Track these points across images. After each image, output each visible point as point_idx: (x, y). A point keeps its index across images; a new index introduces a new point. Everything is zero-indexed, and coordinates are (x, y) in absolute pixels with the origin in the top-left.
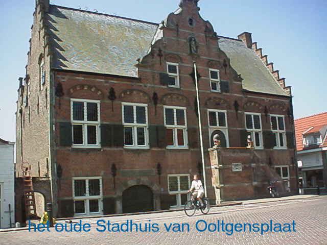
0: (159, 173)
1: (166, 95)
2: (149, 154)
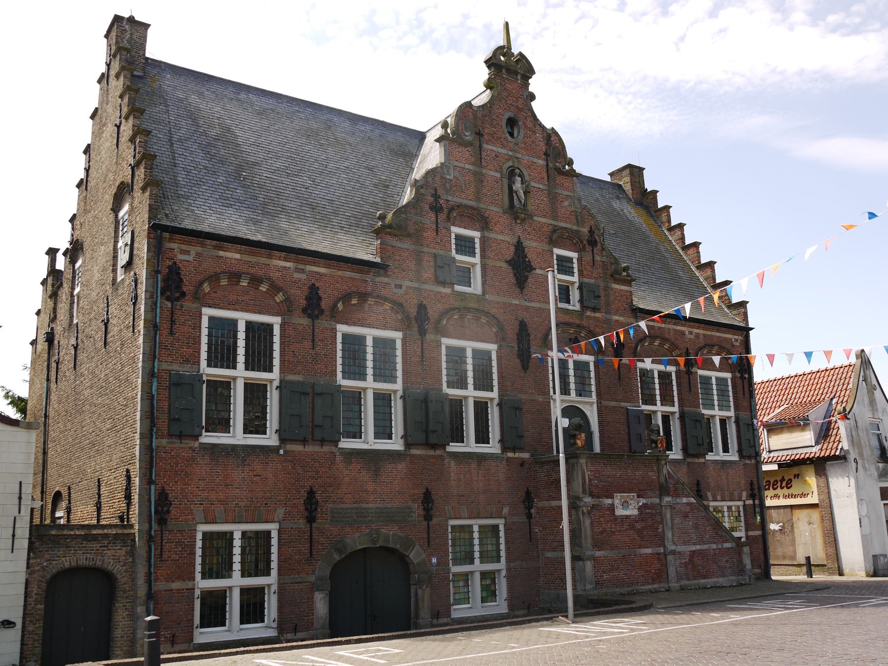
0: (428, 517)
2: (401, 466)
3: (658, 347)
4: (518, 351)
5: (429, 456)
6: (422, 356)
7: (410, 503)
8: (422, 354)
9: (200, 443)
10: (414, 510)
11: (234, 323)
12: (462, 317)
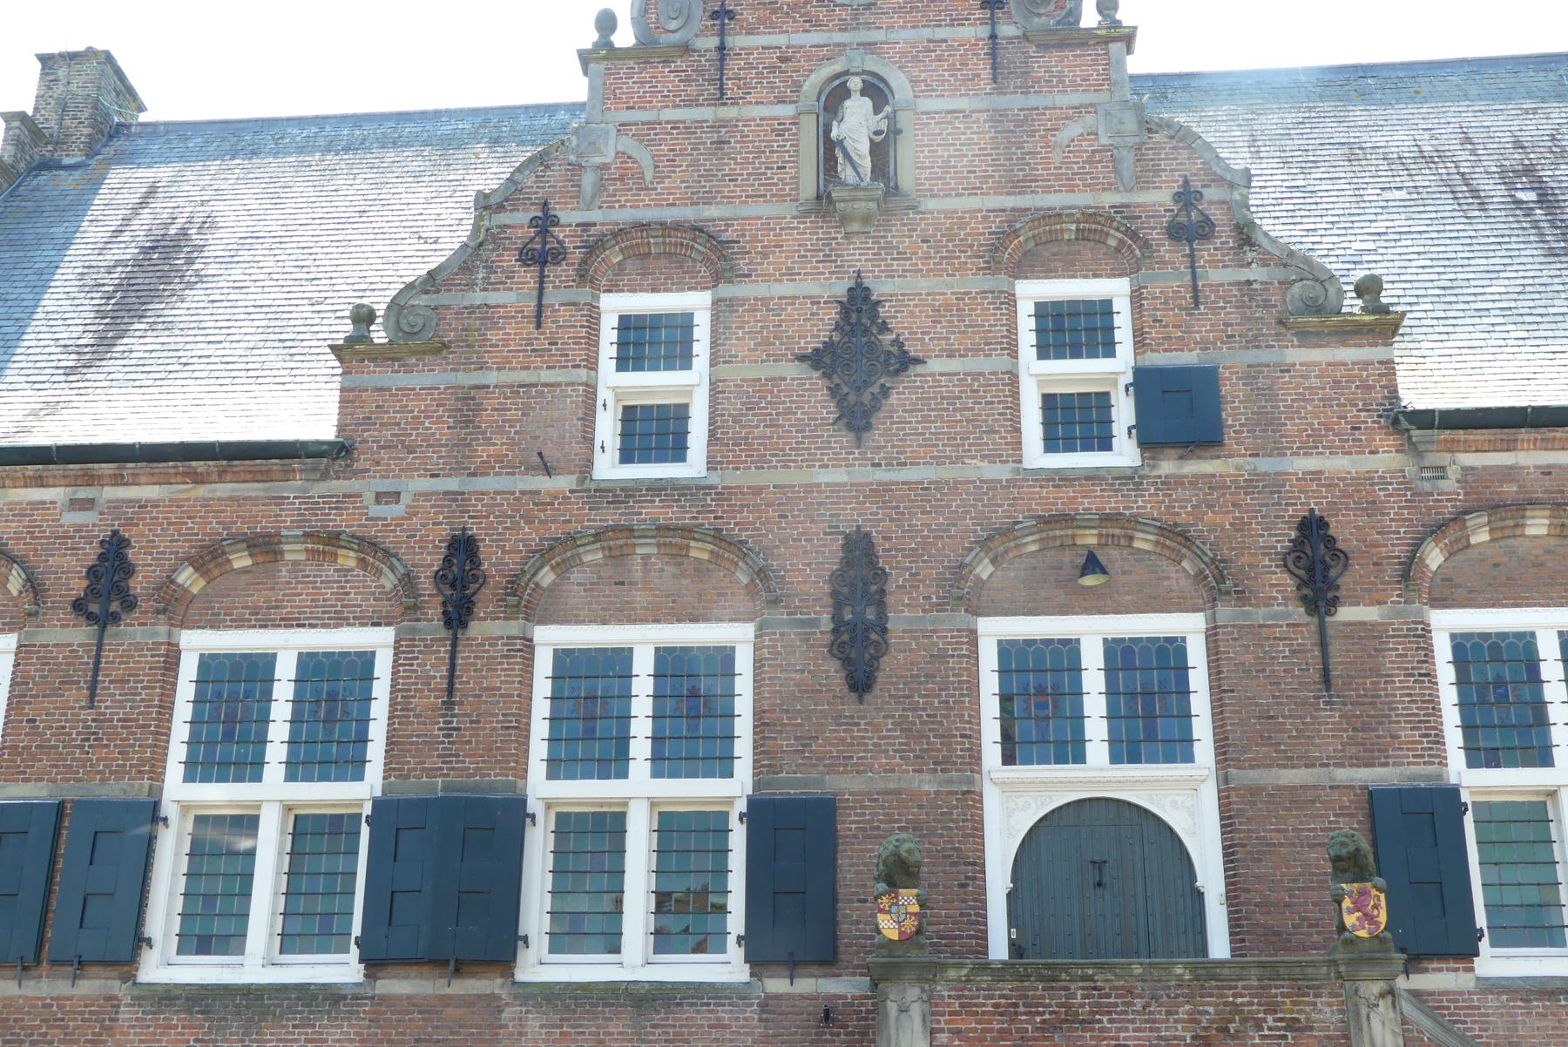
1: (561, 550)
4: (835, 631)
5: (446, 1000)
6: (450, 690)
8: (451, 684)
11: (1069, 649)
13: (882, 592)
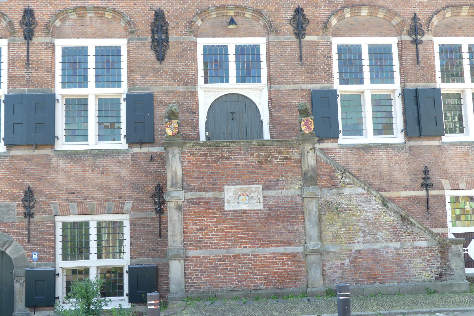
0: (29, 215)
3: (368, 17)
5: (33, 156)
6: (28, 60)
7: (8, 202)
8: (28, 58)
9: (338, 144)
10: (13, 208)
12: (81, 17)
13: (167, 29)
